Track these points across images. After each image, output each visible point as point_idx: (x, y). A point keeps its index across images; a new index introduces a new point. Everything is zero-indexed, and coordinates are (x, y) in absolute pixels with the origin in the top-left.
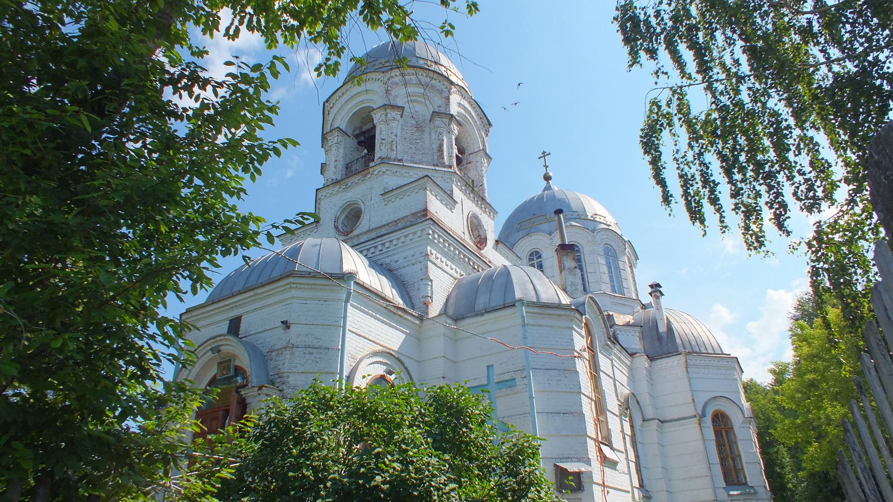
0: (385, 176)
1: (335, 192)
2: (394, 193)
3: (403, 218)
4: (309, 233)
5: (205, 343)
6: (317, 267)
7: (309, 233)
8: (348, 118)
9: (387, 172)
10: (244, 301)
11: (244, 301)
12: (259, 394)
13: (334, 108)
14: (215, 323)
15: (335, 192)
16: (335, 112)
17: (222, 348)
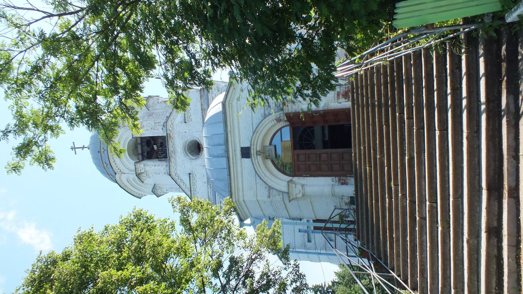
0: (174, 123)
1: (174, 161)
2: (187, 118)
3: (202, 105)
4: (195, 181)
5: (253, 164)
6: (220, 145)
7: (195, 181)
8: (129, 158)
9: (172, 122)
10: (233, 145)
11: (233, 143)
12: (288, 106)
13: (121, 169)
14: (242, 171)
15: (174, 161)
16: (124, 168)
17: (258, 150)
